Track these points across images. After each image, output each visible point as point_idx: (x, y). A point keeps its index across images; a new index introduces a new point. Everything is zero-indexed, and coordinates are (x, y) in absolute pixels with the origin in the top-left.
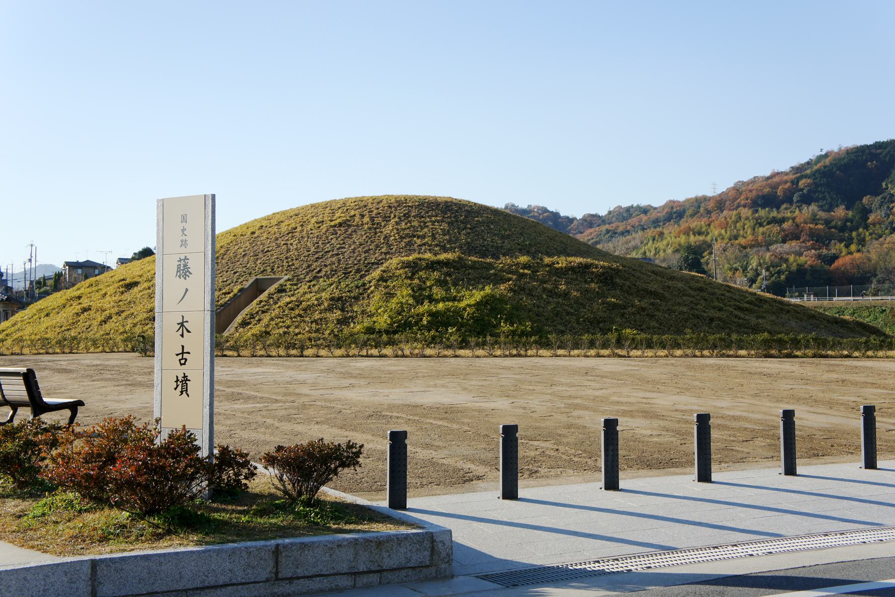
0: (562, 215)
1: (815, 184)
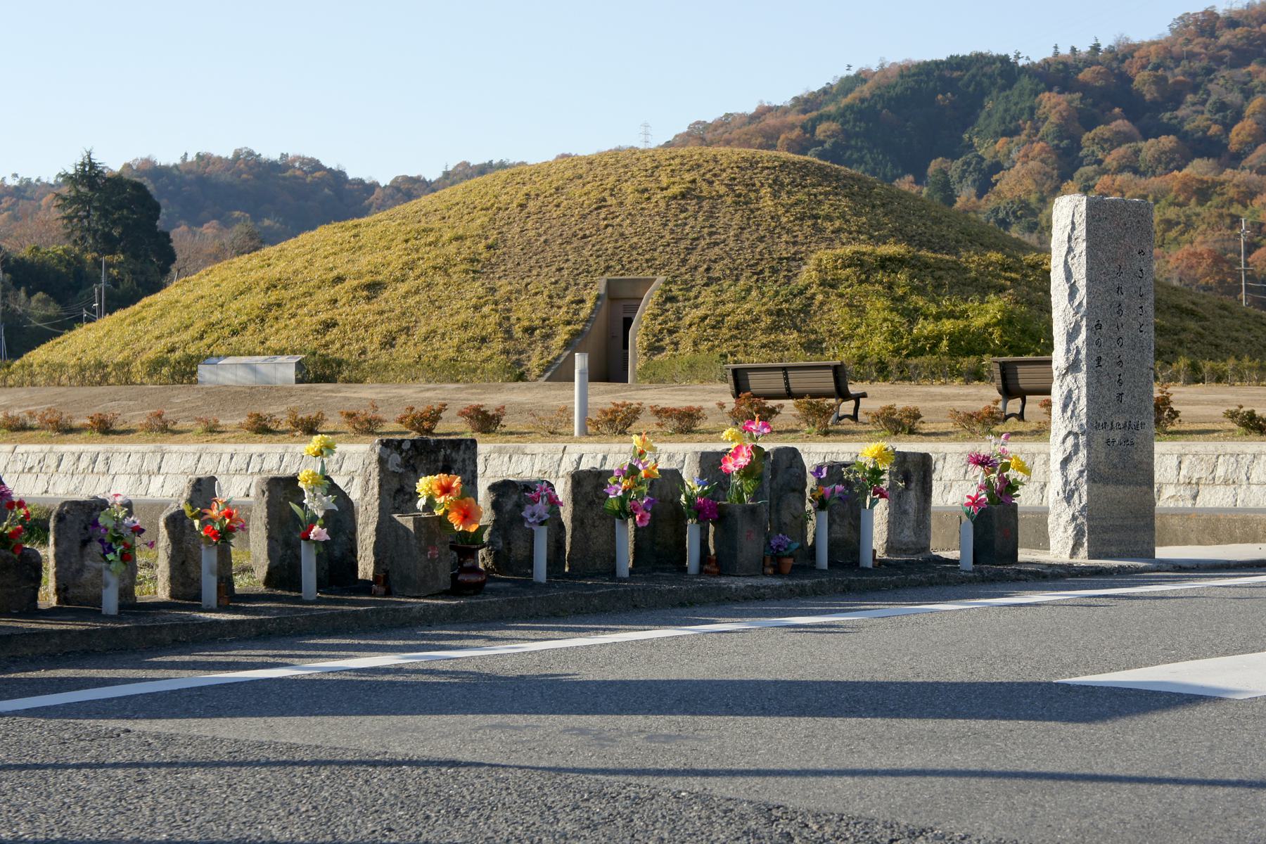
0: (351, 176)
1: (844, 131)
